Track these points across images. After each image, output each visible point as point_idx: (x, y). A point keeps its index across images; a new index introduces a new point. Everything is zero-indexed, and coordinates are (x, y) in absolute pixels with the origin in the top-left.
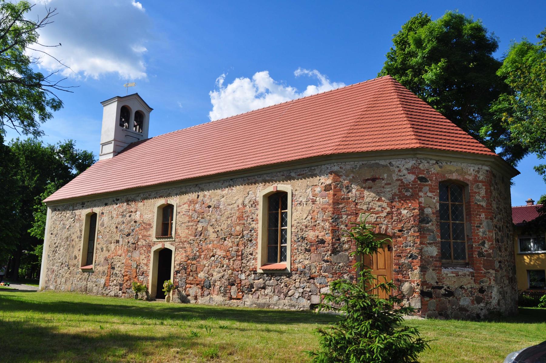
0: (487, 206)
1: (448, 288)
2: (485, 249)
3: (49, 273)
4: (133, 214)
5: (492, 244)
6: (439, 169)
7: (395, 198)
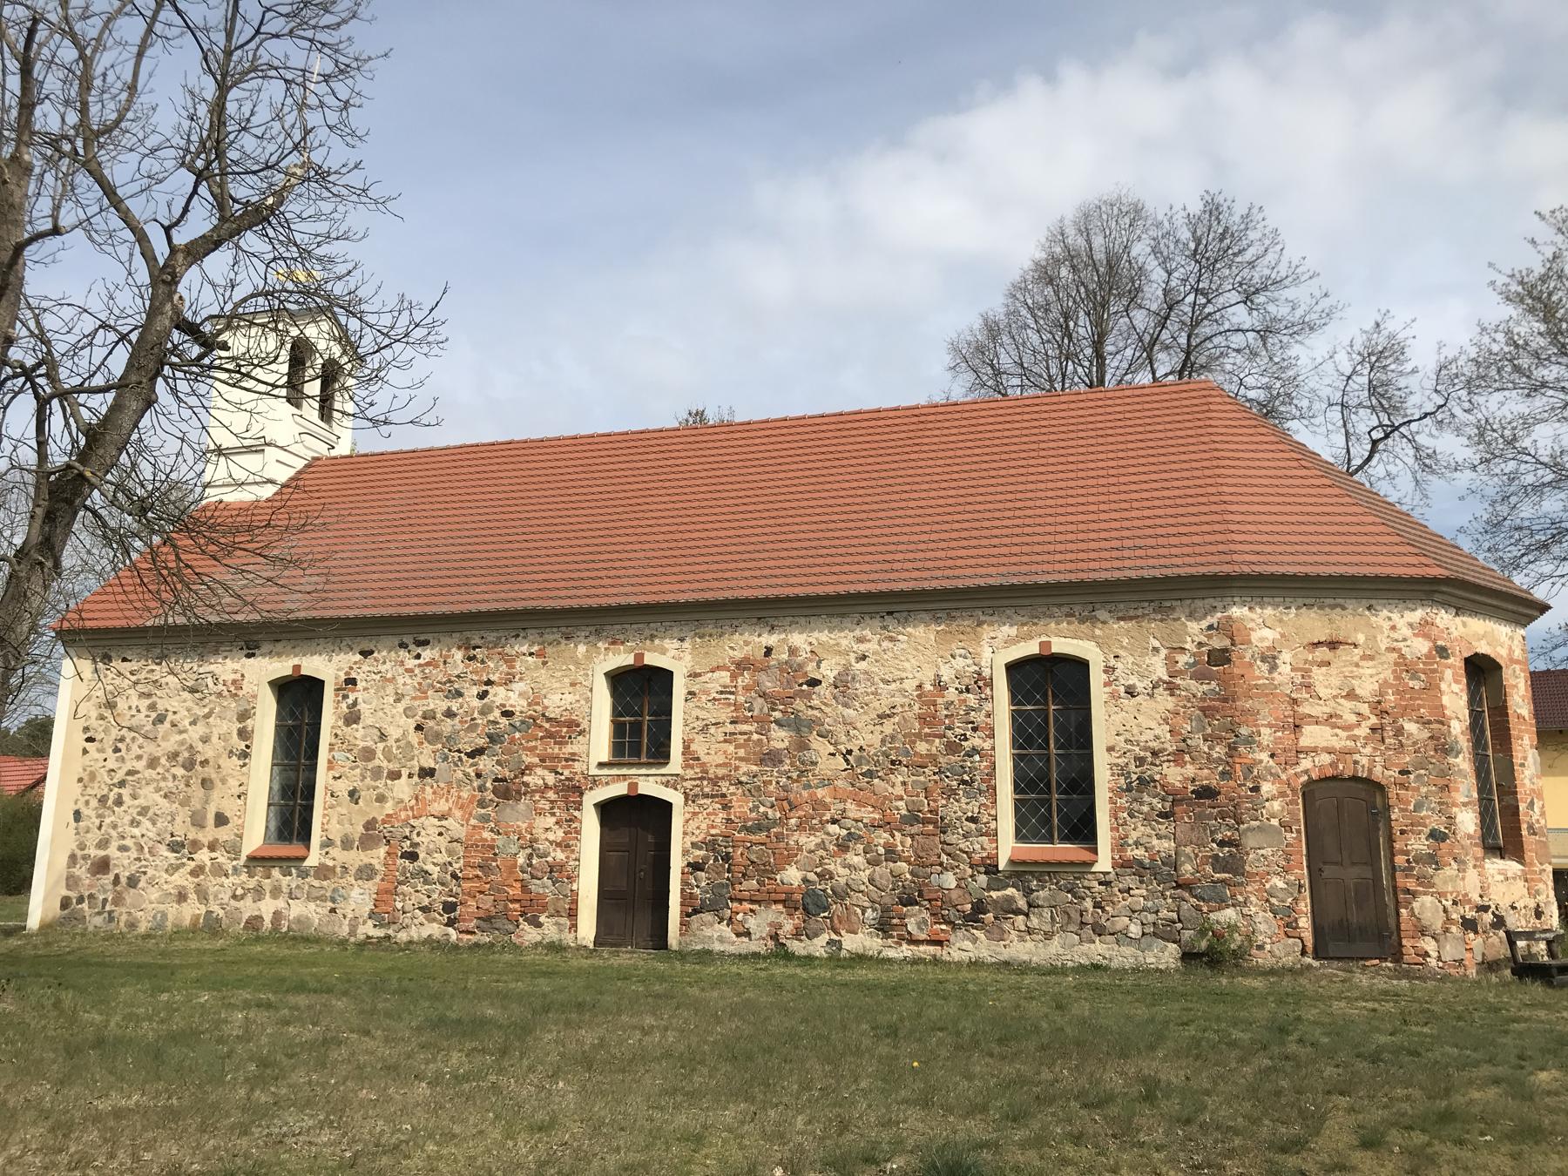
3: (81, 871)
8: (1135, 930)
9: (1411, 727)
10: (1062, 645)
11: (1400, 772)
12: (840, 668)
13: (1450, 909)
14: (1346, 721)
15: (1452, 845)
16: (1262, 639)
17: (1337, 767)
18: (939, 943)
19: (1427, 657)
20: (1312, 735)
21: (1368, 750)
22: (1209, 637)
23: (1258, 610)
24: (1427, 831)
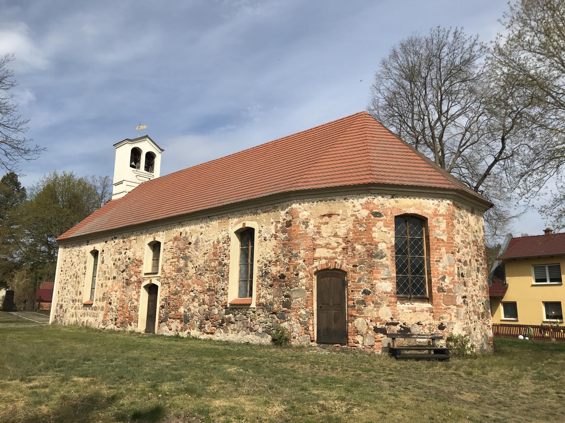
0: (447, 240)
1: (404, 324)
2: (445, 284)
3: (58, 308)
4: (128, 251)
5: (453, 279)
6: (395, 204)
7: (349, 233)
8: (260, 330)
9: (358, 247)
10: (249, 224)
11: (353, 266)
12: (196, 238)
13: (369, 324)
14: (333, 246)
15: (372, 297)
16: (303, 216)
17: (328, 265)
18: (212, 333)
19: (367, 217)
20: (320, 253)
21: (341, 257)
22: (286, 216)
23: (302, 204)
24: (362, 290)
